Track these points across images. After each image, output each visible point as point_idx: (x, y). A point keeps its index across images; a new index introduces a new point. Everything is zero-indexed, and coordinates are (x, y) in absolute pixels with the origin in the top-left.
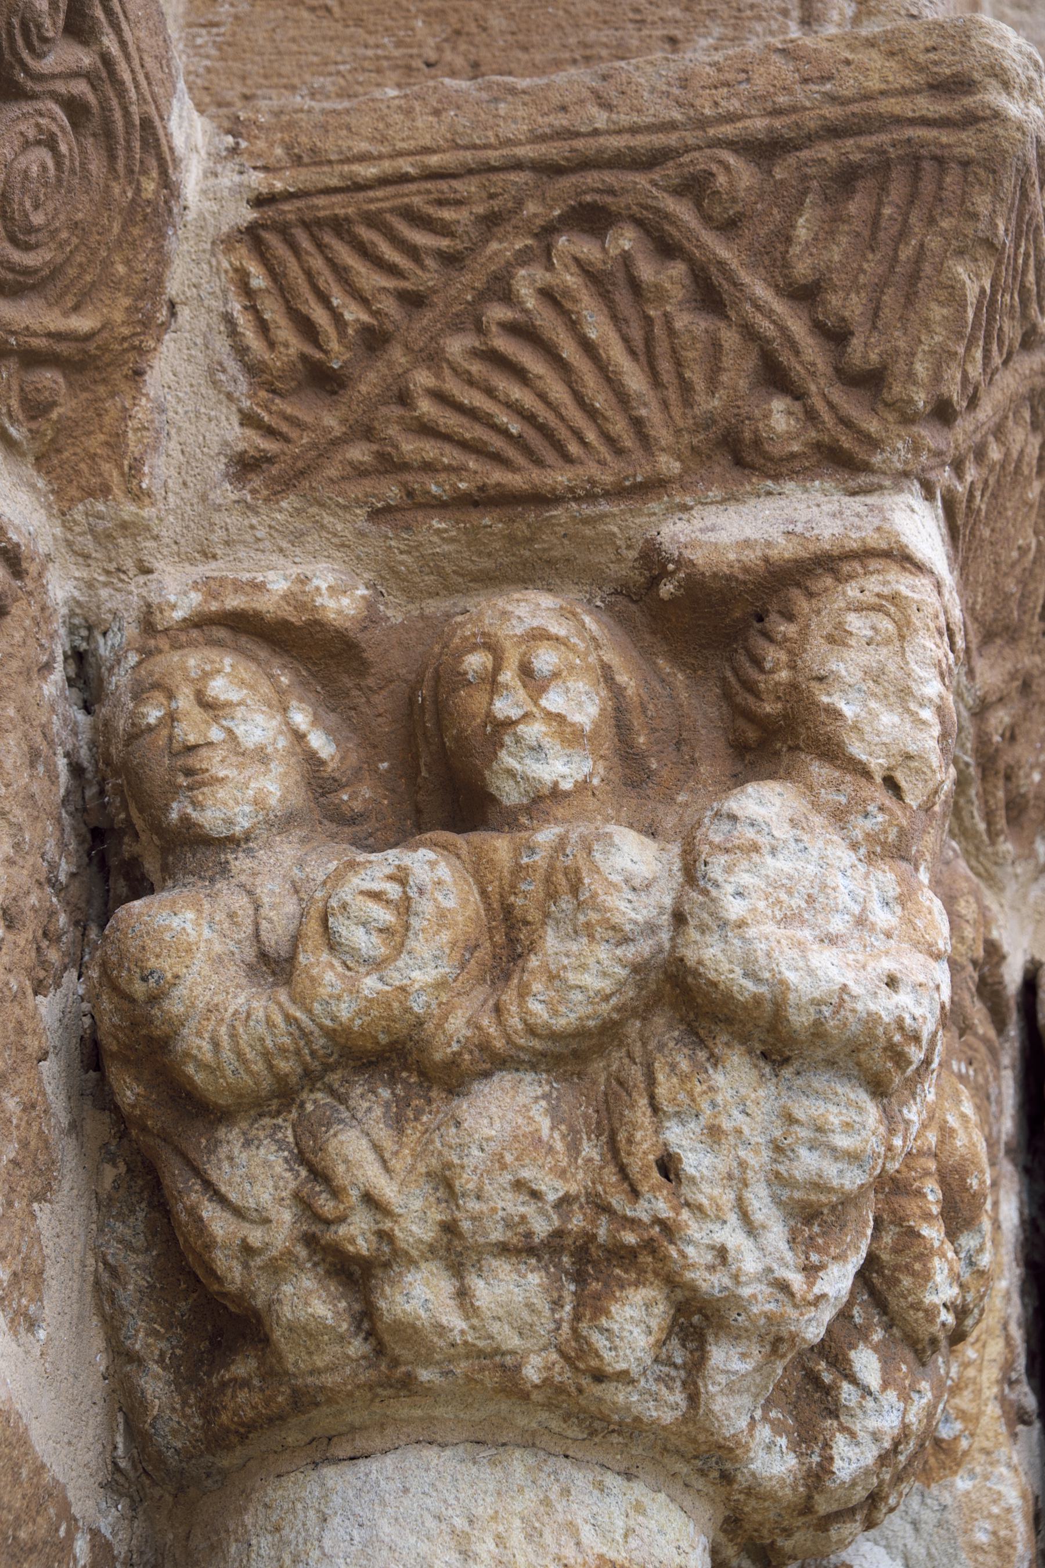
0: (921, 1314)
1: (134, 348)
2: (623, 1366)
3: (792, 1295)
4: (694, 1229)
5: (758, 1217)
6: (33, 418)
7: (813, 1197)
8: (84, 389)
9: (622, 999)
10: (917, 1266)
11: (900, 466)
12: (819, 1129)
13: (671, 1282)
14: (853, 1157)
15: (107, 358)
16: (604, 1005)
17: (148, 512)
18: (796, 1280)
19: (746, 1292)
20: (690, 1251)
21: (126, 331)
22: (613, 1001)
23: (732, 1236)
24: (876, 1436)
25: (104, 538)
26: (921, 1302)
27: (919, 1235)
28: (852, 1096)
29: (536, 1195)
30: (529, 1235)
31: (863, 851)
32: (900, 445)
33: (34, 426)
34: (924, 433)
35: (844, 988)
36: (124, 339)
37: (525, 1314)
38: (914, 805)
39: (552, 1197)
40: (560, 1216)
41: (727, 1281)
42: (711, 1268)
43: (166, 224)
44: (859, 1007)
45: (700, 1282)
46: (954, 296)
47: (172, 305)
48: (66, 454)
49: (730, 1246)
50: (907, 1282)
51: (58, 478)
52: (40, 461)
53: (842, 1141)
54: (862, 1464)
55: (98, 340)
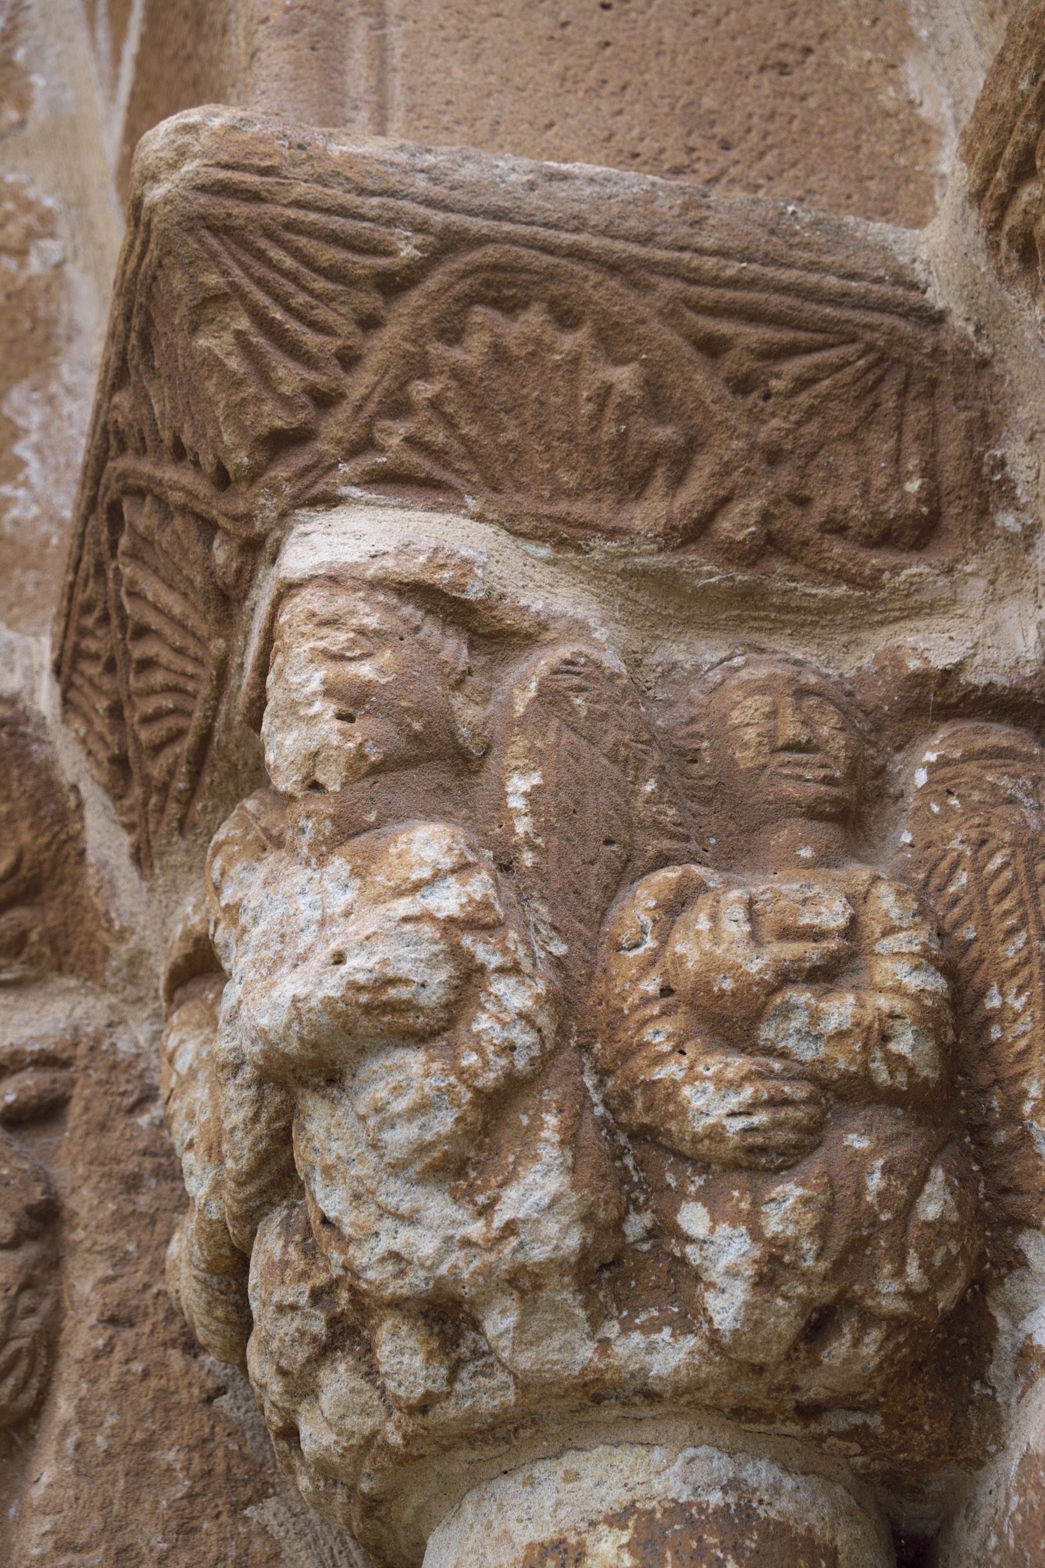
0: (707, 1142)
1: (65, 842)
2: (420, 1391)
3: (476, 1245)
4: (361, 1256)
5: (405, 1207)
6: (19, 953)
7: (428, 1160)
8: (53, 898)
9: (272, 1109)
10: (671, 1108)
11: (274, 514)
12: (377, 1110)
13: (396, 1304)
14: (422, 1108)
15: (47, 867)
16: (258, 1127)
17: (133, 941)
18: (475, 1230)
19: (443, 1269)
20: (371, 1275)
21: (43, 840)
22: (264, 1117)
23: (402, 1239)
24: (732, 1273)
25: (133, 979)
26: (695, 1134)
27: (654, 1083)
28: (388, 1063)
29: (293, 1307)
30: (315, 1339)
31: (313, 861)
32: (262, 500)
33: (23, 957)
34: (272, 474)
35: (295, 1000)
36: (48, 846)
37: (356, 1399)
38: (337, 788)
39: (303, 1301)
40: (322, 1308)
41: (422, 1274)
42: (401, 1274)
43: (25, 746)
44: (314, 1003)
45: (399, 1291)
46: (212, 363)
47: (75, 788)
48: (75, 950)
49: (396, 1248)
50: (673, 1126)
51: (82, 968)
52: (60, 969)
53: (400, 1105)
54: (738, 1304)
55: (26, 863)
